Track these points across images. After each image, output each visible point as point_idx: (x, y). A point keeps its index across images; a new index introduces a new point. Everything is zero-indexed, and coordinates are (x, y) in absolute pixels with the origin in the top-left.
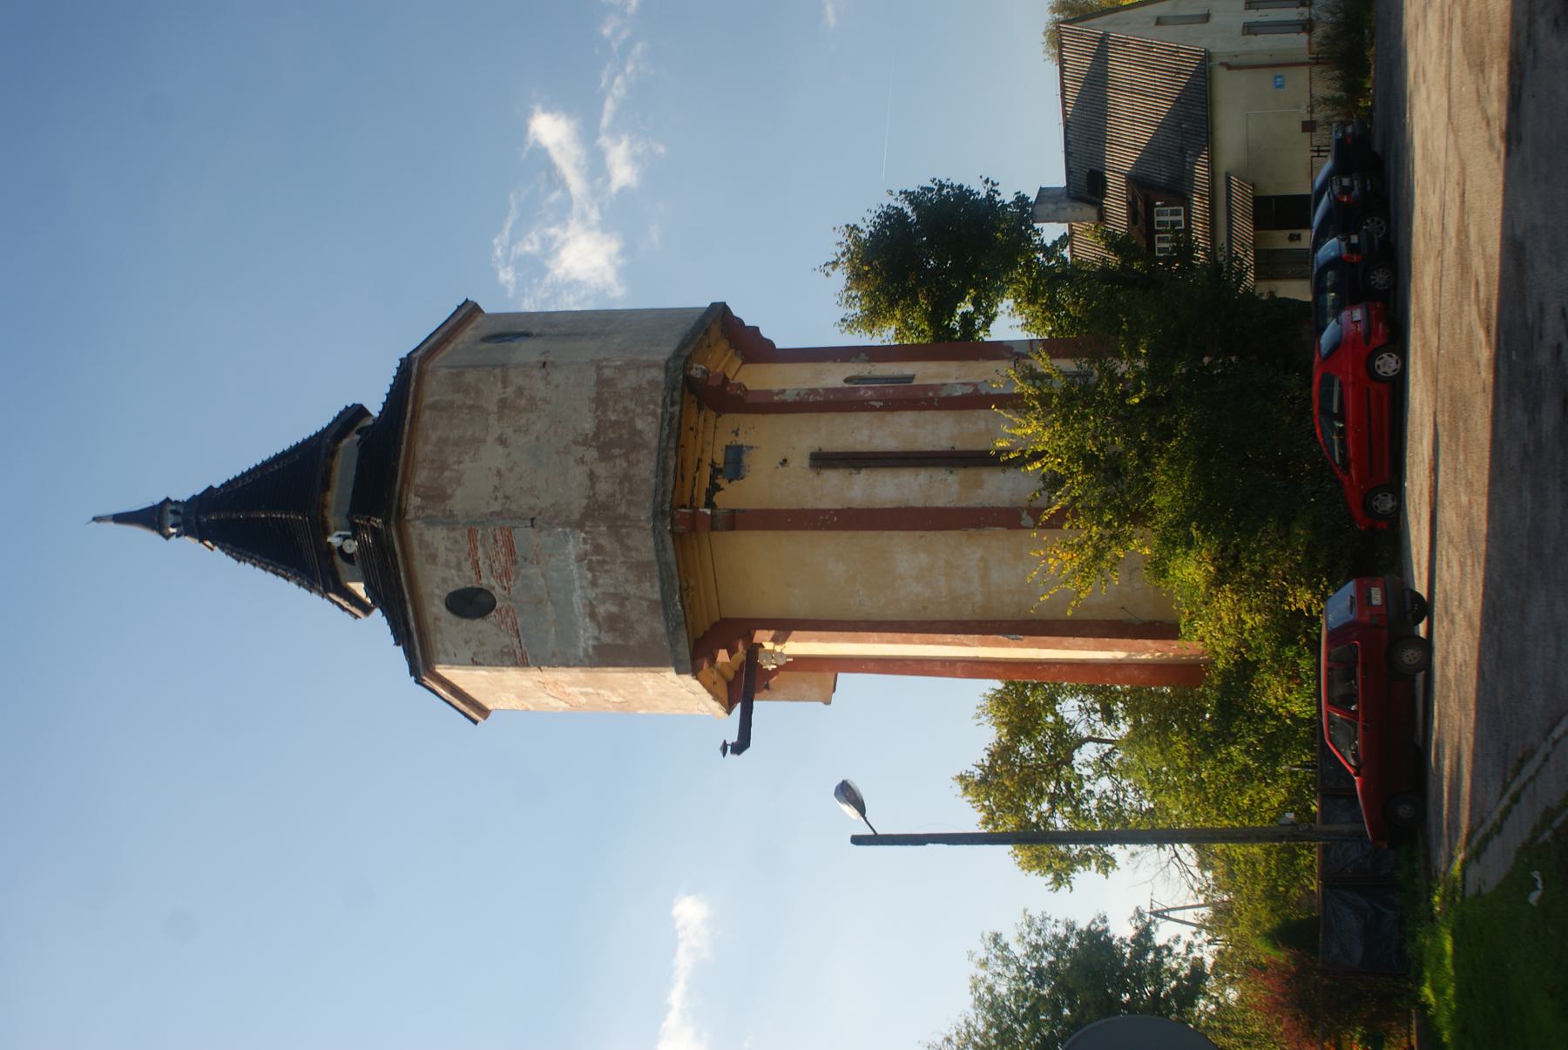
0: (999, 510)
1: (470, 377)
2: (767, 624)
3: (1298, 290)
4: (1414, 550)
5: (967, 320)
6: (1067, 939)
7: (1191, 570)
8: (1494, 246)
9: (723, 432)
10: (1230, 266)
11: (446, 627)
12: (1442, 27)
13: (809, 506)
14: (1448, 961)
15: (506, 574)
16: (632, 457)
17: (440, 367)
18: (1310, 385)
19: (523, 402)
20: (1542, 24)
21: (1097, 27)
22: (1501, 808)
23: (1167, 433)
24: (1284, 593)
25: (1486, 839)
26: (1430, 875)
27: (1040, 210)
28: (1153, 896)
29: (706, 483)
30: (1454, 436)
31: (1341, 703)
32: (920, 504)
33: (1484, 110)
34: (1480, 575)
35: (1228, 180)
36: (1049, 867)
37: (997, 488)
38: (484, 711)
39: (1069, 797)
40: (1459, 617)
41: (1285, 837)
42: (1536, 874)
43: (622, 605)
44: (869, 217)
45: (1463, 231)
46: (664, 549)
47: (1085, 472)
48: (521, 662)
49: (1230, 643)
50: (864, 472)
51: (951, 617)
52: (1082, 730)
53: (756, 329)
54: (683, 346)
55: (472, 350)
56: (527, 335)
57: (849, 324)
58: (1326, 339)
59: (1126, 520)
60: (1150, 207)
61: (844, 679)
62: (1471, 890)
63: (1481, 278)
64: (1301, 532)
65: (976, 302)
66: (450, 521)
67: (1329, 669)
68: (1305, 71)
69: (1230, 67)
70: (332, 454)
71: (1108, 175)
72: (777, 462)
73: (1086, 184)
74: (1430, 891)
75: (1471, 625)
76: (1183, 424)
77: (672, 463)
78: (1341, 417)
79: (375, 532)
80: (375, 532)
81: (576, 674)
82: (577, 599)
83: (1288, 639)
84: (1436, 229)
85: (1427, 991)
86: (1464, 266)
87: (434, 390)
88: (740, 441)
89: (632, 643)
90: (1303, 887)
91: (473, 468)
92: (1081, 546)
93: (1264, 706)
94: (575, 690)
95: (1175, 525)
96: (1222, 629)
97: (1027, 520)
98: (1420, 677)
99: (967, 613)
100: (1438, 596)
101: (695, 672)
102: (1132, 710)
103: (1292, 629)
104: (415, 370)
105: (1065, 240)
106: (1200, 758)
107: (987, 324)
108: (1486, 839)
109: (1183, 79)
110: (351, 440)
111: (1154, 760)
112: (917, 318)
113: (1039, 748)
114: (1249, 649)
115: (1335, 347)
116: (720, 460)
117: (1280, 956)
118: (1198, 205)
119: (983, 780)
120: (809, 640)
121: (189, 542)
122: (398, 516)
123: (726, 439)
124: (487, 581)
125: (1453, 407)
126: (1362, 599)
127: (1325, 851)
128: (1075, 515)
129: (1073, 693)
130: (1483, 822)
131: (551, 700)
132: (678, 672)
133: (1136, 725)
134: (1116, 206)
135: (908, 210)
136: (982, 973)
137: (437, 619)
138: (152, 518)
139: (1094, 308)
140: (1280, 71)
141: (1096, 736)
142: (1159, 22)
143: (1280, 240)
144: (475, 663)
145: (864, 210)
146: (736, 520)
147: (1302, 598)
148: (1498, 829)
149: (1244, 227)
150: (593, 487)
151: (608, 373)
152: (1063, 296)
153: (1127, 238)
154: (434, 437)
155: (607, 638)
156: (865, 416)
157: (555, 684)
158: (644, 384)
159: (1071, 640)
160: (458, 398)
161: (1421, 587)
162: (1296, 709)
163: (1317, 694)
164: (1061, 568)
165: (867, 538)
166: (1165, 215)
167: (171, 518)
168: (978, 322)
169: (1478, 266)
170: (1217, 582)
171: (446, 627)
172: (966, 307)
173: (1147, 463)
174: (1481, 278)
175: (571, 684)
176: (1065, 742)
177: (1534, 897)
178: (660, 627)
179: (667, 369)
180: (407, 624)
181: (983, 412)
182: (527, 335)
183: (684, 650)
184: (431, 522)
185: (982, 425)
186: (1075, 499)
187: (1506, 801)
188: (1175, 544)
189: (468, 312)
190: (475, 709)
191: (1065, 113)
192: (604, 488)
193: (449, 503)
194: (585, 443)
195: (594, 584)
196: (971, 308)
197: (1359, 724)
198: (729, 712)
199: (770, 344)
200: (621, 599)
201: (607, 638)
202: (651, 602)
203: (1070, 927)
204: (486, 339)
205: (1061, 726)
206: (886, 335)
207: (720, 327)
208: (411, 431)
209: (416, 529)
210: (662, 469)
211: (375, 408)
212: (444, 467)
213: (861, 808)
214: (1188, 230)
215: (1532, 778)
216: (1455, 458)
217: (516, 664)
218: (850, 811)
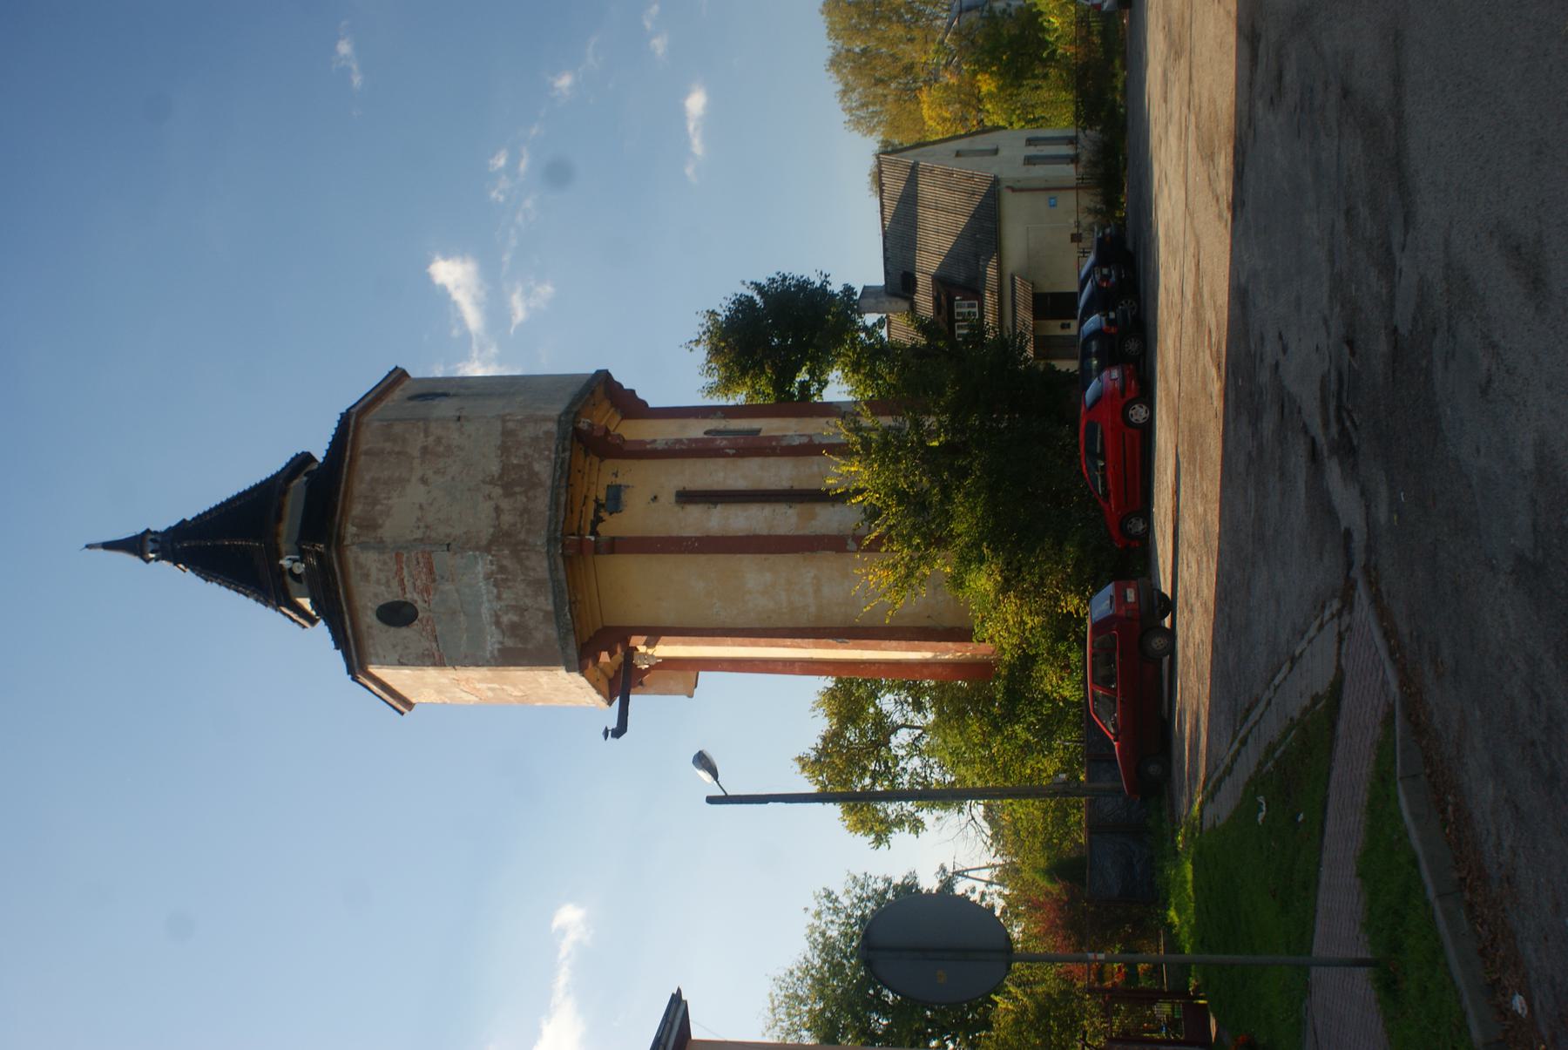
0: (830, 537)
1: (398, 428)
2: (640, 631)
3: (1069, 366)
4: (1160, 561)
5: (804, 386)
6: (886, 891)
7: (983, 581)
8: (1223, 298)
9: (607, 473)
10: (1014, 341)
11: (378, 634)
12: (1180, 138)
13: (674, 534)
14: (1189, 886)
15: (427, 590)
16: (531, 494)
17: (373, 420)
18: (1077, 435)
19: (441, 449)
20: (1260, 105)
21: (909, 159)
22: (1232, 752)
23: (963, 473)
24: (1057, 599)
25: (1220, 780)
26: (1174, 821)
27: (864, 303)
28: (953, 851)
29: (591, 516)
30: (1192, 460)
31: (1105, 682)
32: (765, 532)
33: (1213, 191)
34: (1213, 567)
35: (1013, 279)
36: (871, 829)
37: (828, 519)
38: (409, 705)
39: (888, 771)
40: (1197, 607)
41: (1062, 792)
42: (1261, 799)
43: (522, 615)
44: (725, 303)
45: (1198, 293)
46: (557, 569)
47: (898, 505)
48: (439, 662)
49: (1015, 641)
50: (719, 507)
51: (791, 625)
52: (897, 718)
53: (633, 392)
54: (572, 404)
55: (398, 408)
56: (445, 395)
57: (711, 391)
58: (1090, 394)
59: (931, 544)
60: (951, 301)
61: (705, 677)
62: (1207, 825)
63: (1213, 328)
64: (1071, 550)
65: (811, 372)
66: (380, 546)
67: (1093, 655)
68: (1073, 194)
69: (1013, 190)
70: (284, 492)
71: (918, 275)
72: (649, 499)
73: (900, 283)
74: (1175, 833)
75: (1206, 610)
76: (976, 465)
77: (563, 499)
78: (1102, 456)
79: (319, 556)
80: (319, 556)
81: (484, 672)
82: (485, 611)
83: (1060, 636)
84: (1177, 297)
85: (1172, 913)
86: (1199, 320)
87: (368, 438)
88: (619, 481)
89: (530, 646)
90: (1074, 841)
91: (400, 503)
92: (895, 566)
93: (1042, 692)
94: (483, 686)
95: (969, 546)
96: (1007, 630)
97: (851, 545)
98: (1166, 659)
99: (804, 622)
100: (1180, 592)
101: (582, 670)
102: (937, 702)
103: (1063, 628)
104: (352, 422)
105: (880, 323)
106: (990, 735)
107: (820, 390)
108: (1220, 780)
109: (977, 199)
110: (302, 479)
111: (955, 740)
112: (763, 384)
113: (863, 734)
114: (1030, 645)
115: (1098, 400)
116: (602, 496)
117: (1055, 889)
118: (989, 300)
119: (817, 760)
120: (675, 644)
121: (165, 565)
122: (338, 542)
123: (607, 479)
124: (411, 596)
125: (1192, 437)
126: (1120, 597)
127: (1090, 804)
128: (891, 540)
129: (890, 689)
130: (1217, 767)
131: (464, 695)
132: (568, 670)
133: (940, 713)
134: (925, 302)
135: (757, 298)
136: (817, 923)
137: (369, 627)
138: (135, 545)
139: (905, 377)
140: (1053, 193)
141: (908, 725)
142: (958, 154)
143: (1054, 328)
144: (401, 663)
145: (722, 304)
146: (616, 546)
147: (1071, 603)
148: (1229, 771)
149: (1025, 316)
150: (498, 517)
151: (510, 425)
152: (882, 368)
153: (932, 322)
154: (367, 477)
155: (509, 643)
156: (721, 461)
157: (467, 680)
158: (541, 434)
159: (887, 643)
160: (388, 446)
161: (1166, 589)
162: (1067, 694)
163: (1084, 681)
164: (878, 585)
165: (722, 560)
166: (963, 307)
167: (151, 546)
168: (813, 389)
169: (1210, 317)
170: (1004, 588)
171: (378, 634)
172: (803, 376)
173: (946, 496)
174: (1213, 328)
175: (480, 681)
176: (884, 729)
177: (1261, 816)
178: (553, 632)
179: (559, 422)
180: (344, 631)
181: (816, 459)
182: (445, 395)
183: (573, 652)
184: (365, 546)
185: (815, 469)
186: (890, 527)
187: (1236, 745)
188: (970, 562)
189: (398, 377)
190: (402, 703)
191: (883, 226)
192: (507, 519)
193: (380, 532)
194: (492, 482)
195: (499, 597)
196: (807, 377)
197: (1118, 700)
198: (610, 704)
199: (644, 403)
200: (521, 610)
201: (509, 643)
202: (547, 613)
203: (888, 881)
204: (411, 398)
205: (880, 716)
206: (739, 398)
207: (603, 390)
208: (349, 473)
209: (353, 553)
210: (555, 504)
211: (320, 455)
212: (376, 502)
213: (715, 775)
214: (982, 316)
215: (1256, 723)
216: (1193, 475)
217: (434, 665)
218: (705, 776)
